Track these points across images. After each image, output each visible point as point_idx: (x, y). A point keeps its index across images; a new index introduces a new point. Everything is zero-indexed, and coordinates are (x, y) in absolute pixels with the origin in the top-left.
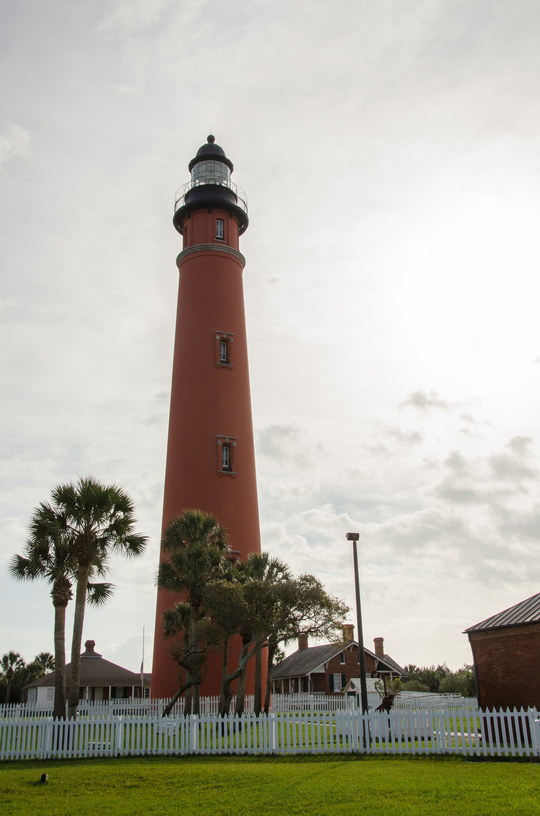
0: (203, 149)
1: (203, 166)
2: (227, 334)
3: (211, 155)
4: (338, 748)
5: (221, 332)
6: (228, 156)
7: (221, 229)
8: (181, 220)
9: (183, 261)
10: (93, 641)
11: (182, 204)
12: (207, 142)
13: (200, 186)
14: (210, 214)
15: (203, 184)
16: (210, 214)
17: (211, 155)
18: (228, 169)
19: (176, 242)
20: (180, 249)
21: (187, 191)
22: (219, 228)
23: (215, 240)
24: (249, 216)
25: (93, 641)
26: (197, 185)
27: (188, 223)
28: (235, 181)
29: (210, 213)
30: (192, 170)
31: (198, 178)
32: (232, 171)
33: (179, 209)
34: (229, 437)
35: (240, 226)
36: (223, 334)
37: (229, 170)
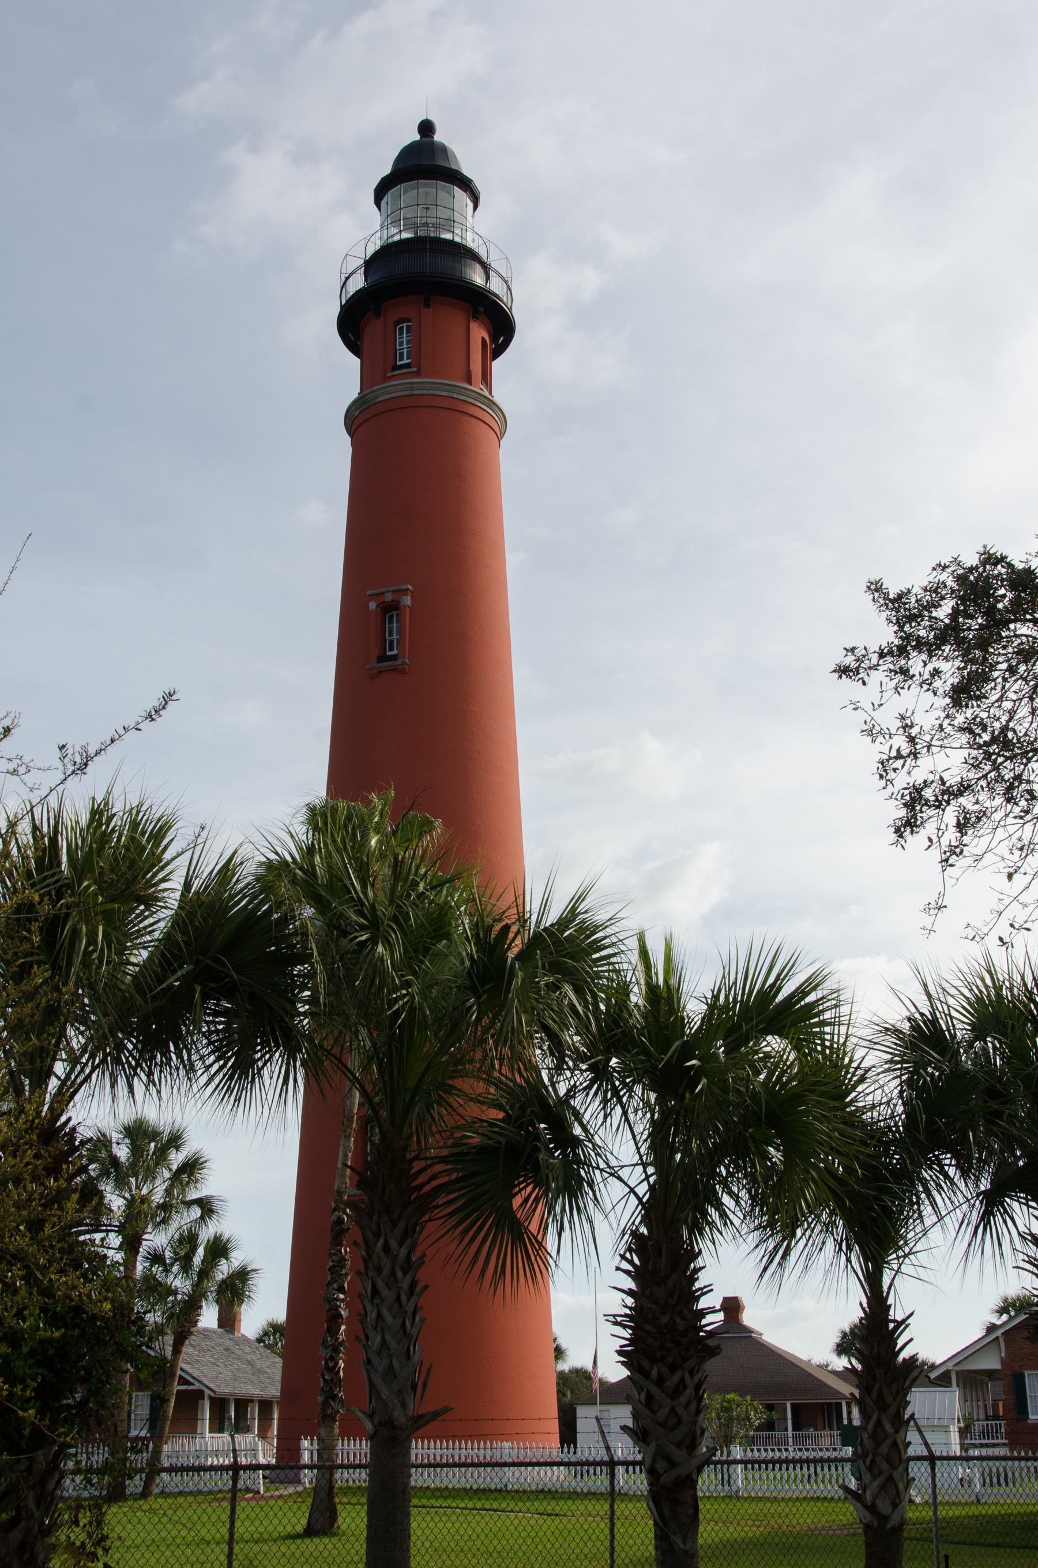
0: (408, 153)
1: (405, 194)
2: (394, 591)
3: (423, 165)
4: (551, 1506)
5: (379, 591)
6: (466, 171)
7: (401, 344)
8: (355, 322)
9: (357, 420)
10: (725, 1298)
11: (358, 283)
12: (417, 137)
13: (402, 242)
14: (422, 308)
15: (405, 235)
16: (422, 308)
17: (423, 165)
18: (469, 201)
19: (343, 375)
20: (352, 390)
21: (371, 251)
22: (403, 342)
23: (389, 375)
24: (518, 315)
25: (725, 1298)
26: (397, 238)
27: (373, 330)
28: (476, 227)
29: (427, 305)
30: (383, 203)
31: (396, 222)
32: (476, 207)
33: (352, 296)
34: (395, 588)
35: (494, 338)
36: (383, 593)
37: (471, 205)
